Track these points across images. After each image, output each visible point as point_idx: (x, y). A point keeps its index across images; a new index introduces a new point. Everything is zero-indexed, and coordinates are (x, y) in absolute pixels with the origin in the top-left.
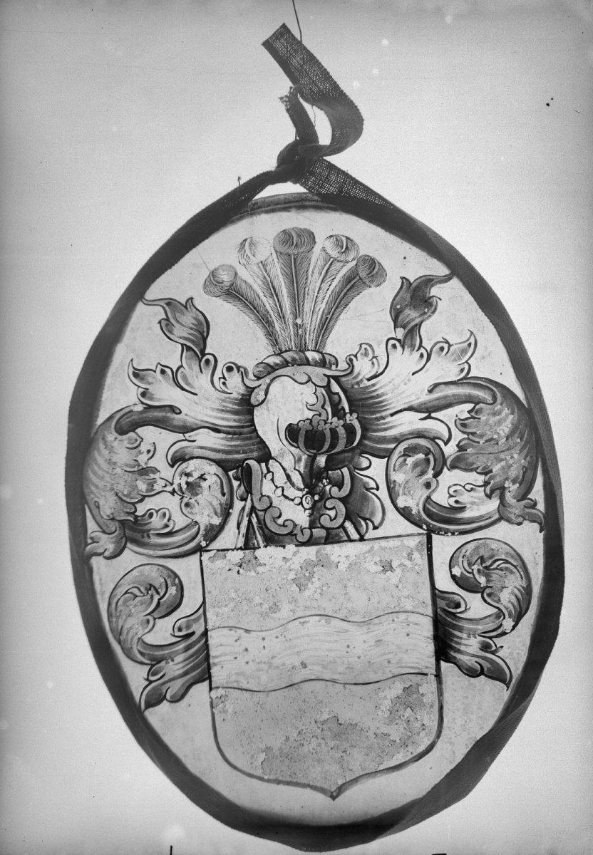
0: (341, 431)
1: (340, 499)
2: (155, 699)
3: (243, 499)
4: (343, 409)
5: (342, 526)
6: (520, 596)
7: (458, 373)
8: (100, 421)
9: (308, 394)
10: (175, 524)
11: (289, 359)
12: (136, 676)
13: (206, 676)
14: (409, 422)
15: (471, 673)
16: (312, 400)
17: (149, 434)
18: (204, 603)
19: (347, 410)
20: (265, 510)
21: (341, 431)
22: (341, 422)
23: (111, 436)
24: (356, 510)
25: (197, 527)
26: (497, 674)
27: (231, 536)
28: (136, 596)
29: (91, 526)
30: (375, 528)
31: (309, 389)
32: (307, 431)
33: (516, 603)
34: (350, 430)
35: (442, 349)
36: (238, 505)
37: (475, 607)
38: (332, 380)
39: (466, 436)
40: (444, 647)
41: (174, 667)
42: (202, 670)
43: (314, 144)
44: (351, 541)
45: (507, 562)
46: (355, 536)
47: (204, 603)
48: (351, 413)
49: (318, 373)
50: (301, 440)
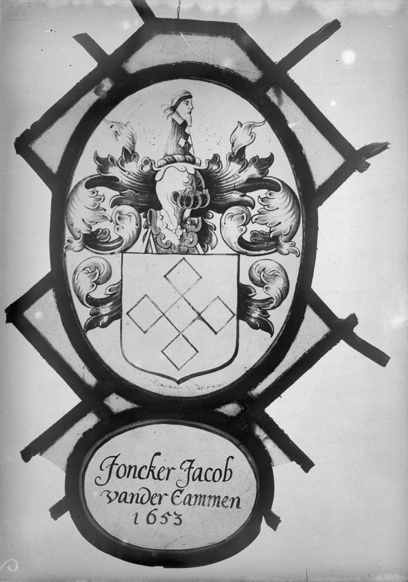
0: (200, 199)
1: (196, 233)
2: (91, 325)
3: (146, 227)
4: (202, 186)
5: (195, 246)
6: (282, 290)
7: (250, 139)
8: (74, 183)
9: (185, 178)
10: (110, 238)
11: (187, 159)
12: (84, 314)
13: (119, 316)
14: (236, 196)
15: (254, 327)
16: (187, 180)
17: (102, 190)
18: (122, 280)
19: (204, 187)
20: (157, 235)
21: (200, 199)
22: (201, 193)
23: (82, 189)
24: (204, 236)
25: (122, 241)
26: (267, 327)
27: (140, 246)
28: (89, 272)
29: (68, 235)
30: (253, 208)
31: (186, 174)
32: (182, 196)
33: (280, 295)
34: (204, 197)
35: (292, 244)
36: (143, 231)
37: (260, 294)
38: (197, 171)
39: (263, 207)
40: (243, 313)
41: (105, 310)
42: (116, 315)
43: (255, 163)
44: (199, 254)
45: (278, 272)
46: (201, 251)
47: (122, 280)
48: (205, 189)
49: (191, 168)
50: (179, 199)
